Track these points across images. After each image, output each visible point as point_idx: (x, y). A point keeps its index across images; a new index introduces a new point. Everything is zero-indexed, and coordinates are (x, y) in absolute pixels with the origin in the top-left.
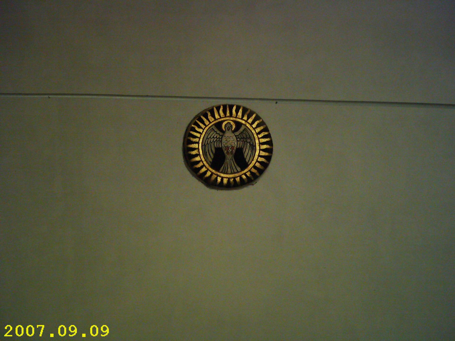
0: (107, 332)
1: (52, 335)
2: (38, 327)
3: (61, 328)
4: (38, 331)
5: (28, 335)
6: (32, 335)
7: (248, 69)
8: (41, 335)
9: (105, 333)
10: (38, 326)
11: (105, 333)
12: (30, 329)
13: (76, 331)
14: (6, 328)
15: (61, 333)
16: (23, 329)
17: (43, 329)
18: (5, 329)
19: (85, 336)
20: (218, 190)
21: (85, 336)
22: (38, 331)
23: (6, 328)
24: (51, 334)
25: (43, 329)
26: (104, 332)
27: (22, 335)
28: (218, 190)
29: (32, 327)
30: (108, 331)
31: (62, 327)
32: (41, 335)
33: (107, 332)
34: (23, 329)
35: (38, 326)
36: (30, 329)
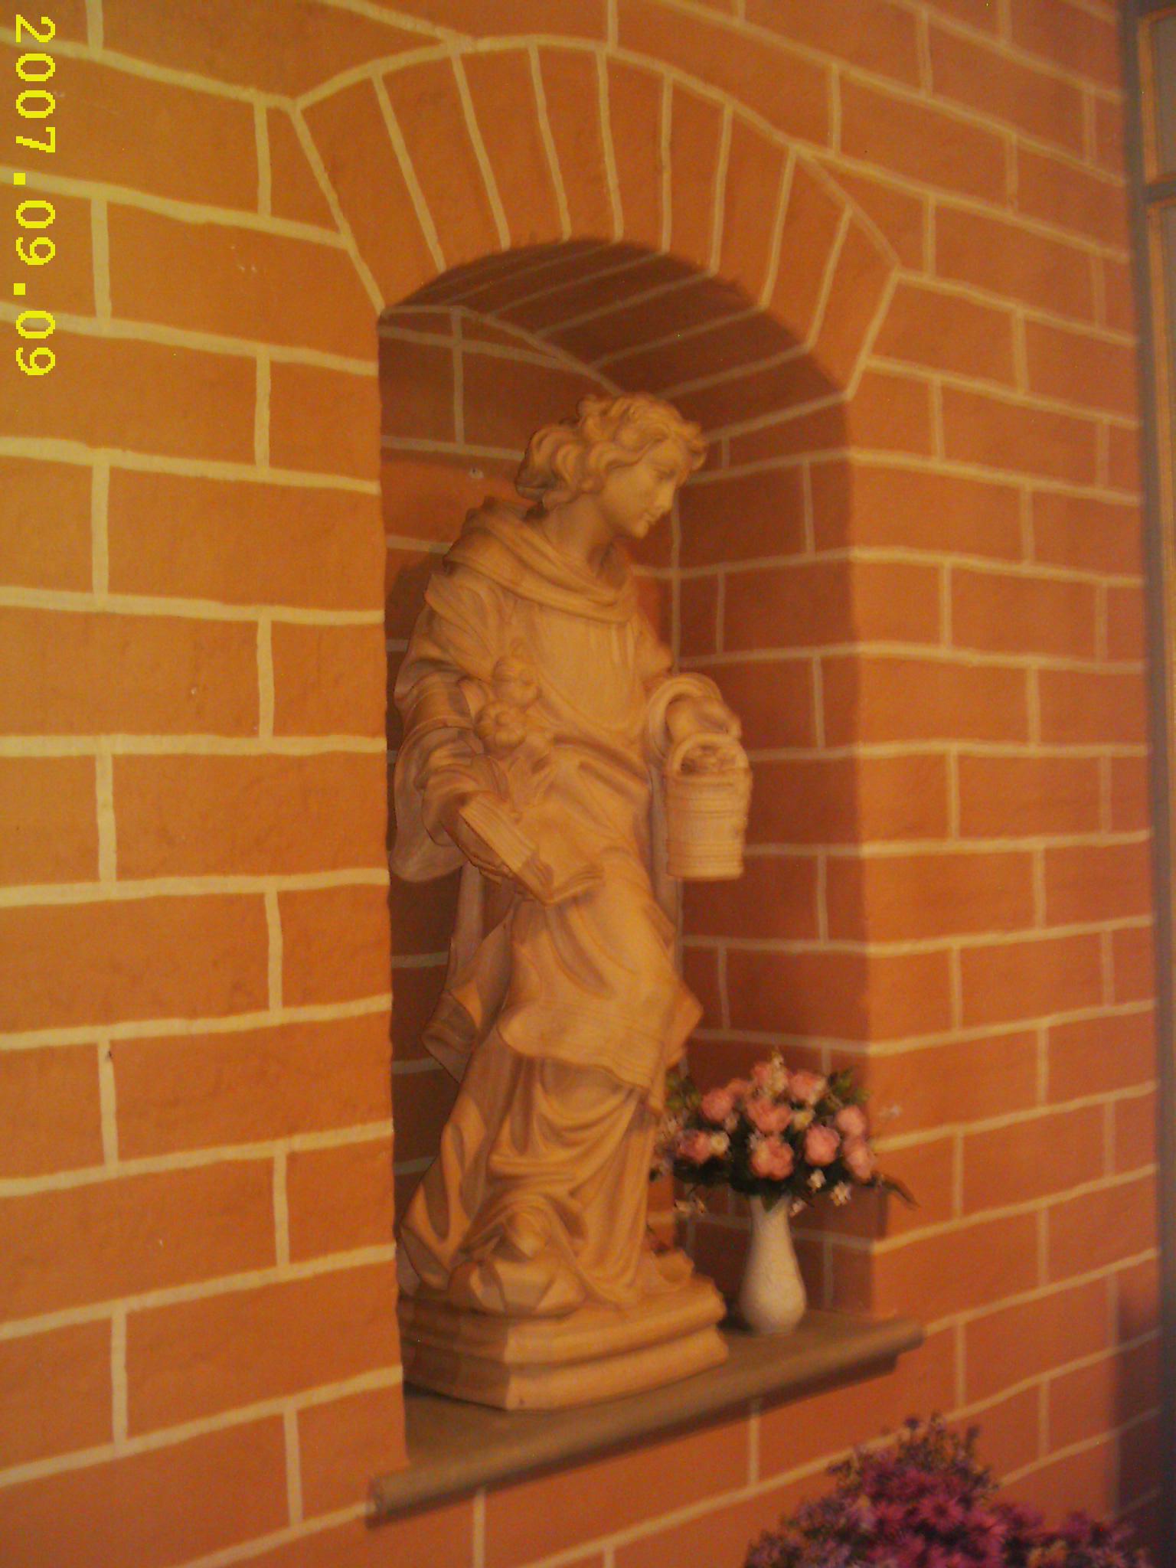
0: (30, 367)
1: (19, 289)
2: (48, 129)
3: (44, 99)
4: (36, 130)
5: (22, 97)
6: (22, 111)
7: (18, 829)
8: (20, 140)
9: (27, 252)
10: (51, 130)
11: (27, 362)
12: (41, 104)
13: (35, 260)
14: (45, 20)
15: (27, 99)
16: (42, 78)
17: (42, 147)
18: (43, 18)
19: (23, 285)
20: (522, 1402)
21: (23, 285)
22: (36, 130)
23: (45, 20)
24: (24, 293)
25: (42, 147)
26: (32, 247)
27: (22, 75)
28: (522, 1402)
29: (50, 110)
30: (35, 371)
31: (49, 68)
32: (20, 140)
33: (31, 367)
34: (42, 78)
35: (51, 130)
36: (41, 104)
